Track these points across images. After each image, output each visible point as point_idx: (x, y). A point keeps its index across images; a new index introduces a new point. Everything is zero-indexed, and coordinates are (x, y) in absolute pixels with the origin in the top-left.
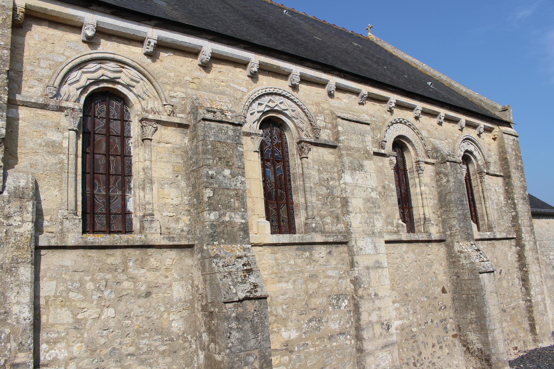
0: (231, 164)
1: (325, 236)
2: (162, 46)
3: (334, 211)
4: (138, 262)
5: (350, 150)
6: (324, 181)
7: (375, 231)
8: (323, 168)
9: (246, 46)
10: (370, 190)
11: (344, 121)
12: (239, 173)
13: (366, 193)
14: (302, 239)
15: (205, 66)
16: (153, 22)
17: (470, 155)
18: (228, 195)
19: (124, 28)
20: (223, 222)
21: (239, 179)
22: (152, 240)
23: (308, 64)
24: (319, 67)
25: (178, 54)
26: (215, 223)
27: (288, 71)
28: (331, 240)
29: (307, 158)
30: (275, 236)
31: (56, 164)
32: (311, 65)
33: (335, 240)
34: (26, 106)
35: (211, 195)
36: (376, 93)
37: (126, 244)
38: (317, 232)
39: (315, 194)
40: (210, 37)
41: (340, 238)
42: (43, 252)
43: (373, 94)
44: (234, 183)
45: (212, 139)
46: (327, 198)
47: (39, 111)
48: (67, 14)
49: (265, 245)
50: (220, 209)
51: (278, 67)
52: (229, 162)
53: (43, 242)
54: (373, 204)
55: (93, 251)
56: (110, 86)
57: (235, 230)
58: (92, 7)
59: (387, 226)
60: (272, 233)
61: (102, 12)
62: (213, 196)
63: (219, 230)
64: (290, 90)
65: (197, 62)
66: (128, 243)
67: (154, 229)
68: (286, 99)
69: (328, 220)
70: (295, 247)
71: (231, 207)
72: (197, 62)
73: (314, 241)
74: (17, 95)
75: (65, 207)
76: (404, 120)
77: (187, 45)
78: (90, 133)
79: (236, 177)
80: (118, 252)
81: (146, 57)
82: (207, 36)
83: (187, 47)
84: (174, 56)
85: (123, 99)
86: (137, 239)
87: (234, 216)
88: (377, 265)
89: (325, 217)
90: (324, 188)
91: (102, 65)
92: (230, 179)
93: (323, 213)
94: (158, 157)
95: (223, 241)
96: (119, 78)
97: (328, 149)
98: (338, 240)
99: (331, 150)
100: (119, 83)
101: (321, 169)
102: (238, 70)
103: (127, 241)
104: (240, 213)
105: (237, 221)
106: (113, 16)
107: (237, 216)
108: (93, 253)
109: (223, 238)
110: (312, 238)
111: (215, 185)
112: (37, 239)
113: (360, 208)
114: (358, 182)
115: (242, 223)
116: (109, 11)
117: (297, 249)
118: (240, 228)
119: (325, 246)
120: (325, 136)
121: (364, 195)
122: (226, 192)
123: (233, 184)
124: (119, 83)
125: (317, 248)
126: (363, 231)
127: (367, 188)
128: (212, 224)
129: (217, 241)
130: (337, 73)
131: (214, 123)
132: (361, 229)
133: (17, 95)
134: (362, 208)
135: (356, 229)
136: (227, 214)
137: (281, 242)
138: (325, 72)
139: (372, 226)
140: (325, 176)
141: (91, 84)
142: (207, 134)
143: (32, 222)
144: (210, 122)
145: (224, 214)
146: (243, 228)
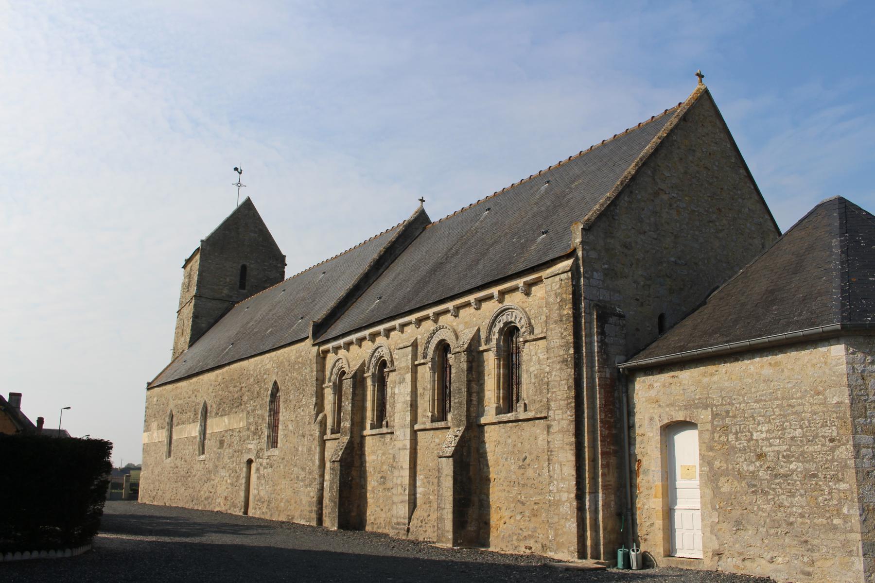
53: (416, 427)
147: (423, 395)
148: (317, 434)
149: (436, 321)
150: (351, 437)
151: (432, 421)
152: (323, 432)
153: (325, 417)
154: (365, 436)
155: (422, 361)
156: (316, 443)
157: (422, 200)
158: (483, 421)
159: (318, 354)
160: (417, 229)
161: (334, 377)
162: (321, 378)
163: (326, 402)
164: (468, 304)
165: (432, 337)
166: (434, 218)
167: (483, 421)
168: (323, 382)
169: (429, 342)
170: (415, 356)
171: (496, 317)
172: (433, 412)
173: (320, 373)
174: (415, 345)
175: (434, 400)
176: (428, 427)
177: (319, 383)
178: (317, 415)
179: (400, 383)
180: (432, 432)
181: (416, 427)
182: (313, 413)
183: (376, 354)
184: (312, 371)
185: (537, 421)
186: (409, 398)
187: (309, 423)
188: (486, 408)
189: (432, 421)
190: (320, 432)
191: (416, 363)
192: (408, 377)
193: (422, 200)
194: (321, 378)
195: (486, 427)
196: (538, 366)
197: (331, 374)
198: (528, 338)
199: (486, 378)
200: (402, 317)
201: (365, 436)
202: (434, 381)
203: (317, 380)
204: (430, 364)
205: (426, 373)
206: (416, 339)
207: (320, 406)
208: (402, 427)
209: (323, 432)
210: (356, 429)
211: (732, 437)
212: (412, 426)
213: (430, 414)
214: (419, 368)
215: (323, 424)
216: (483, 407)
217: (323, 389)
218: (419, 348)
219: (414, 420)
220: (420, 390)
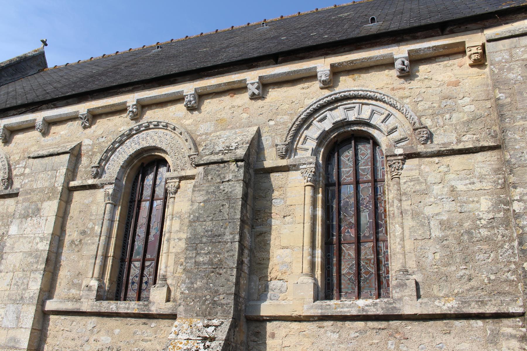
2: (202, 96)
5: (30, 194)
7: (26, 295)
10: (38, 240)
13: (31, 245)
17: (365, 129)
19: (289, 73)
36: (102, 105)
42: (52, 317)
43: (98, 108)
51: (352, 62)
53: (50, 305)
54: (36, 258)
59: (69, 290)
60: (316, 298)
61: (16, 114)
64: (327, 92)
65: (394, 73)
72: (466, 61)
74: (264, 162)
76: (151, 122)
78: (334, 185)
81: (402, 80)
85: (368, 138)
88: (11, 344)
113: (15, 266)
114: (25, 232)
121: (26, 248)
126: (8, 296)
127: (35, 238)
130: (44, 106)
133: (264, 162)
134: (18, 265)
138: (452, 33)
139: (24, 289)
147: (78, 245)
149: (136, 117)
151: (99, 298)
155: (90, 182)
157: (45, 43)
158: (266, 309)
160: (32, 68)
165: (122, 143)
166: (50, 64)
167: (266, 309)
169: (113, 150)
170: (72, 171)
171: (316, 111)
172: (101, 279)
174: (76, 154)
175: (105, 257)
176: (85, 307)
179: (26, 216)
180: (94, 320)
181: (50, 305)
185: (458, 323)
186: (44, 246)
188: (272, 284)
189: (99, 298)
191: (72, 184)
192: (51, 208)
193: (45, 43)
196: (449, 205)
198: (421, 148)
199: (276, 222)
202: (112, 221)
204: (110, 189)
205: (95, 209)
206: (80, 145)
208: (15, 302)
211: (184, 264)
212: (41, 303)
213: (94, 284)
214: (76, 195)
216: (264, 279)
218: (84, 161)
219: (48, 290)
220: (71, 233)
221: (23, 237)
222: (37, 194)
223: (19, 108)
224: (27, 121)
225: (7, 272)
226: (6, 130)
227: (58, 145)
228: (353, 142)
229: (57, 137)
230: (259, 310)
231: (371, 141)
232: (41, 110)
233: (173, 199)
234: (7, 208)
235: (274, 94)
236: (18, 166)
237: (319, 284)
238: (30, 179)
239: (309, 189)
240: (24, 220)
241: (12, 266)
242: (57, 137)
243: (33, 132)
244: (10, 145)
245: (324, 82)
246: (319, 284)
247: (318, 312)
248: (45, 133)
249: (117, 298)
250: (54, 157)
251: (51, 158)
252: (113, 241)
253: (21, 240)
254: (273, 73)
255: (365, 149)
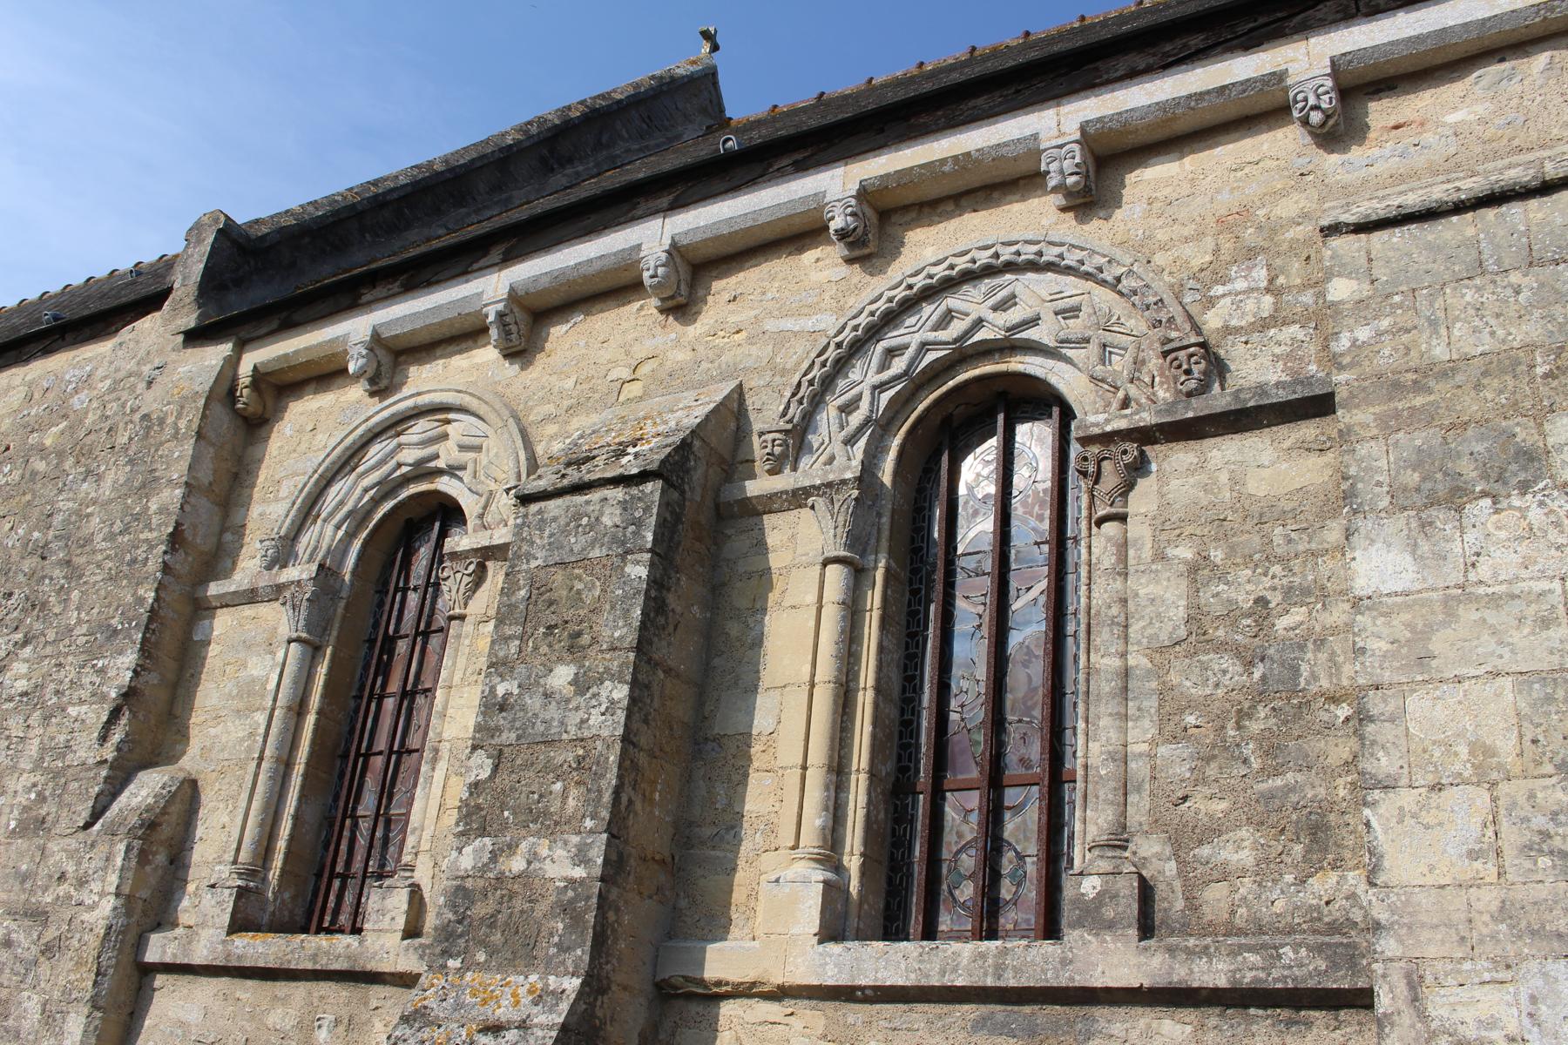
0: (585, 639)
1: (1171, 950)
3: (1289, 789)
4: (341, 1029)
5: (1418, 387)
6: (1231, 615)
8: (1232, 550)
9: (798, 156)
11: (1378, 238)
12: (607, 670)
14: (999, 970)
15: (681, 307)
16: (496, 254)
18: (548, 768)
20: (500, 879)
21: (604, 694)
22: (376, 953)
23: (1122, 65)
24: (1196, 41)
25: (602, 305)
26: (469, 884)
27: (1021, 149)
28: (1214, 973)
29: (1122, 518)
30: (834, 948)
31: (242, 740)
32: (1141, 61)
33: (1247, 978)
34: (227, 606)
35: (485, 774)
37: (309, 966)
38: (1111, 926)
39: (1152, 703)
40: (665, 201)
41: (1297, 965)
42: (160, 980)
44: (581, 714)
45: (539, 562)
46: (1243, 715)
47: (248, 611)
48: (320, 345)
49: (781, 994)
50: (504, 826)
51: (964, 161)
52: (579, 634)
53: (158, 948)
55: (249, 983)
56: (423, 487)
57: (542, 908)
58: (365, 299)
62: (492, 777)
63: (480, 910)
66: (315, 963)
67: (388, 917)
68: (1030, 275)
69: (1239, 849)
70: (970, 1011)
71: (546, 814)
73: (1080, 981)
75: (229, 857)
77: (597, 266)
79: (594, 689)
80: (299, 990)
82: (653, 204)
83: (603, 273)
84: (589, 319)
85: (1036, 400)
86: (340, 950)
87: (544, 852)
89: (1213, 831)
90: (1227, 662)
91: (403, 439)
92: (568, 701)
93: (1206, 806)
94: (470, 670)
95: (481, 957)
96: (437, 456)
97: (1282, 430)
98: (1276, 978)
99: (1308, 430)
100: (439, 472)
101: (1217, 555)
102: (809, 256)
103: (314, 957)
104: (575, 839)
105: (551, 870)
106: (410, 295)
107: (560, 853)
108: (247, 990)
109: (483, 943)
110: (1065, 962)
111: (504, 736)
112: (140, 944)
114: (1484, 571)
115: (572, 882)
116: (396, 287)
117: (979, 1025)
118: (559, 903)
119: (1190, 1014)
120: (1256, 370)
122: (542, 754)
123: (574, 719)
124: (439, 472)
125: (1117, 1028)
126: (1504, 912)
128: (458, 888)
129: (458, 955)
131: (559, 501)
132: (1488, 899)
135: (1423, 899)
136: (524, 846)
137: (863, 981)
140: (1243, 589)
141: (376, 502)
142: (525, 548)
143: (117, 895)
144: (542, 504)
145: (512, 848)
146: (572, 901)
148: (101, 909)
149: (381, 386)
150: (594, 985)
151: (240, 924)
152: (153, 898)
153: (188, 796)
154: (714, 996)
156: (74, 974)
158: (721, 962)
159: (224, 390)
161: (322, 535)
162: (201, 539)
163: (211, 694)
164: (617, 287)
167: (721, 962)
168: (217, 560)
173: (203, 503)
177: (182, 563)
178: (120, 776)
181: (158, 948)
182: (89, 751)
183: (971, 302)
184: (149, 485)
187: (33, 825)
189: (240, 924)
190: (127, 901)
194: (201, 539)
195: (729, 1010)
197: (308, 511)
200: (734, 188)
201: (714, 996)
203: (176, 539)
207: (153, 716)
209: (153, 898)
210: (636, 915)
215: (164, 847)
217: (201, 609)
221: (1472, 598)
222: (1478, 387)
223: (1171, 39)
224: (1222, 90)
225: (1437, 787)
226: (381, 353)
227: (1451, 165)
228: (1001, 418)
229: (1429, 138)
230: (701, 964)
231: (1056, 411)
232: (369, 305)
233: (1110, 528)
234: (1234, 481)
235: (1147, 182)
236: (1219, 290)
237: (854, 887)
238: (1385, 323)
239: (836, 574)
240: (1439, 515)
241: (1463, 751)
242: (1429, 138)
243: (1279, 133)
244: (1119, 214)
245: (1068, 193)
246: (854, 887)
247: (832, 976)
248: (681, 307)
249: (892, 929)
250: (1514, 210)
251: (1490, 214)
252: (865, 700)
253: (1468, 614)
254: (321, 340)
255: (1034, 439)
